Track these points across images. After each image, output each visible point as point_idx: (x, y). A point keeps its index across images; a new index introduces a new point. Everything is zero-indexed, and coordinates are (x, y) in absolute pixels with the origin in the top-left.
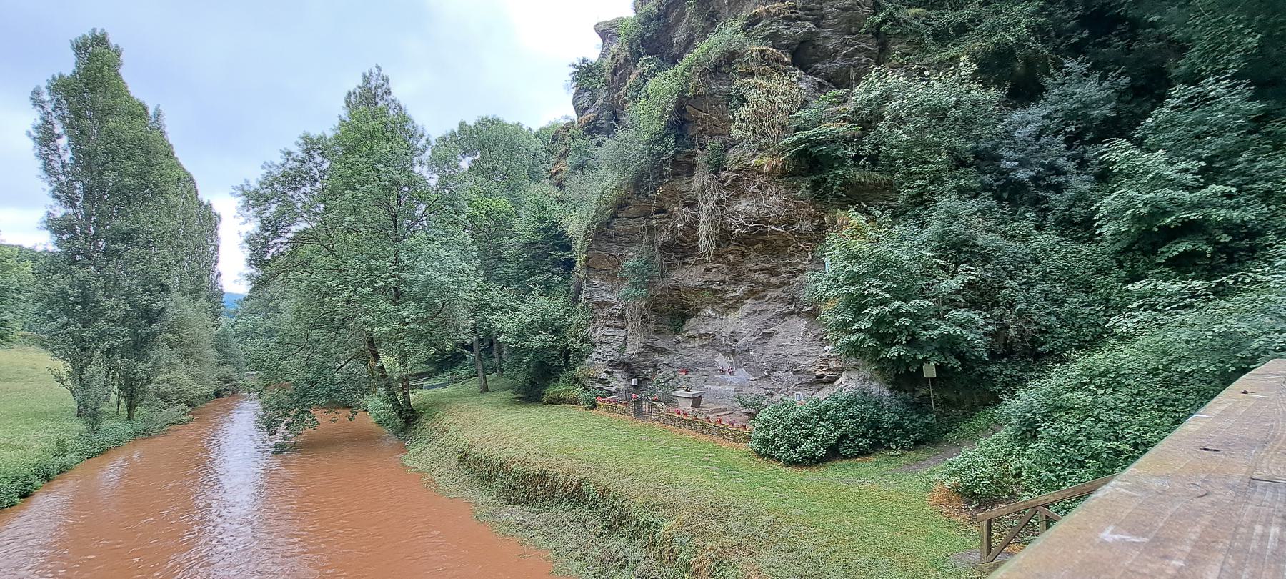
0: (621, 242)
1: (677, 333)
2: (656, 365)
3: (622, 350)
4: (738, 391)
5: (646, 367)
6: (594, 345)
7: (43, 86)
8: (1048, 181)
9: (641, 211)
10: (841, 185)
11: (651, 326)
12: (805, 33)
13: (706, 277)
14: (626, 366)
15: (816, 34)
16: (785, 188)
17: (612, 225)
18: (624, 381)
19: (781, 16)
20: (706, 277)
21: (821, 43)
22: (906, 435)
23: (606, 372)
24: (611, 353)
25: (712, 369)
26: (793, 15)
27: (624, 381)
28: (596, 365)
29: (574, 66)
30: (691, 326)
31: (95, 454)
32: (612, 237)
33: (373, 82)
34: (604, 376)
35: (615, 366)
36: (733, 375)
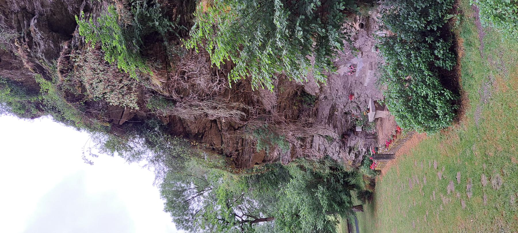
0: (242, 145)
1: (317, 99)
2: (346, 113)
3: (331, 140)
5: (347, 121)
6: (327, 157)
7: (188, 231)
9: (216, 135)
10: (170, 20)
11: (311, 120)
12: (40, 30)
14: (345, 137)
15: (41, 15)
16: (180, 61)
17: (229, 154)
18: (357, 138)
19: (29, 50)
21: (48, 9)
23: (349, 153)
25: (350, 78)
26: (27, 40)
27: (357, 138)
32: (239, 154)
34: (353, 156)
35: (344, 145)
36: (356, 65)
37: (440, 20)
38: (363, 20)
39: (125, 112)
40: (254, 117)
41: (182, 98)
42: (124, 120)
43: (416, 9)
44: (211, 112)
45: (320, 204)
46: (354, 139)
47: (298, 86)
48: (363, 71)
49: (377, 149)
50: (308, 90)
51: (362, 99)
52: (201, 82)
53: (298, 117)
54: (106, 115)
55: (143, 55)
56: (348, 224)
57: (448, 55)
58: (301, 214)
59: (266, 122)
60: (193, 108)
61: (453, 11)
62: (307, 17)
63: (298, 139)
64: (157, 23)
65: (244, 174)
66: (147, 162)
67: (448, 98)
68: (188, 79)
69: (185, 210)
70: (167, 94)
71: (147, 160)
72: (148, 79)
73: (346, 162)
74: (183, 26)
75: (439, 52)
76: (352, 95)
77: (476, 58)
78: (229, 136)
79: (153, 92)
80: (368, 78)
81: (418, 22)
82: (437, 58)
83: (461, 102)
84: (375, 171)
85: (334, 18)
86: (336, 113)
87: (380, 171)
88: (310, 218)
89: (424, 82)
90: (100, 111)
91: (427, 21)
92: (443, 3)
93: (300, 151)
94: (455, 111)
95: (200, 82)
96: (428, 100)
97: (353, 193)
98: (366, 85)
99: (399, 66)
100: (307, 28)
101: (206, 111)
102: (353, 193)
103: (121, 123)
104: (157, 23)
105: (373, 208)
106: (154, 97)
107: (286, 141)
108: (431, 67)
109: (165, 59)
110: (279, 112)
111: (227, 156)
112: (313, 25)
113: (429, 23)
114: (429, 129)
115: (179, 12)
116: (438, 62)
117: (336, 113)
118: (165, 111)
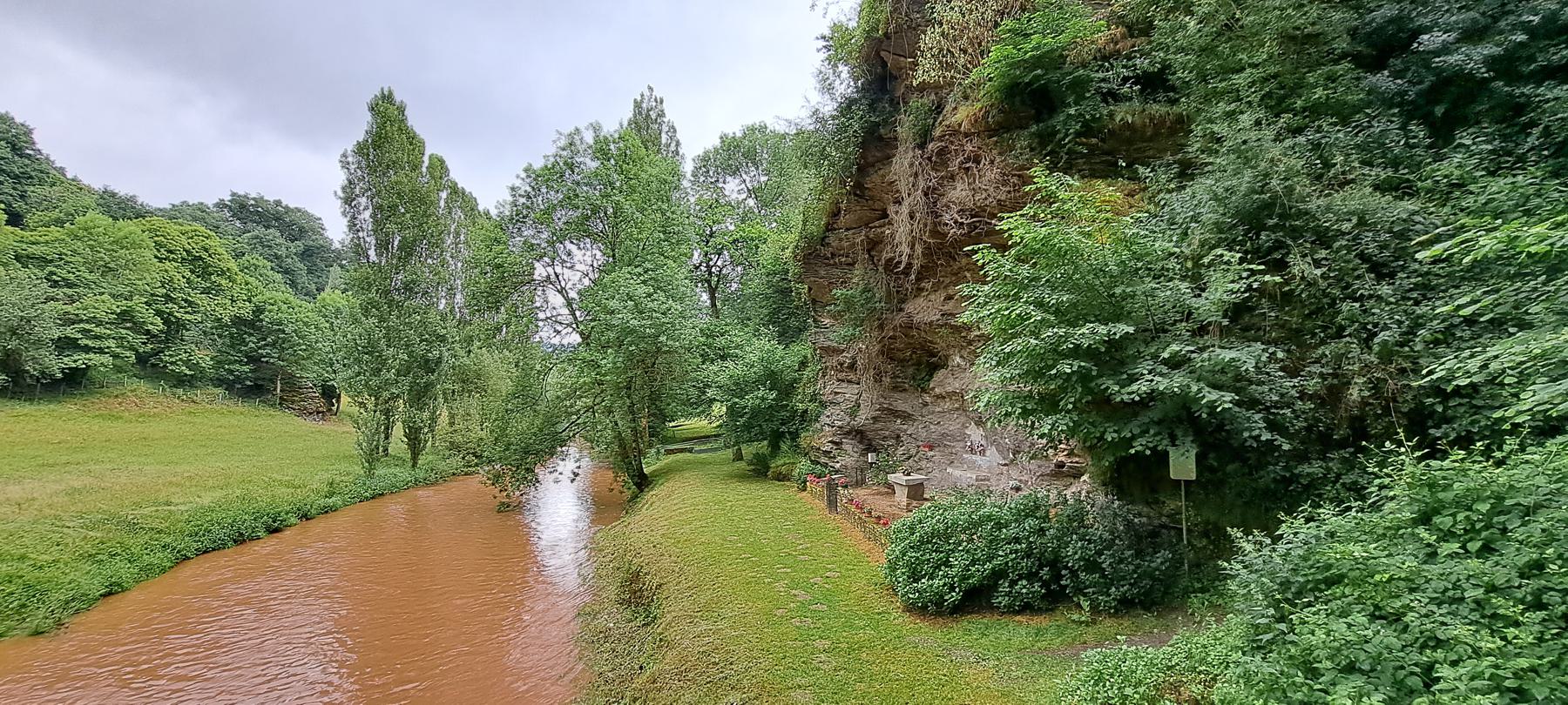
1: (924, 390)
2: (898, 436)
3: (853, 413)
4: (982, 480)
5: (885, 438)
6: (823, 405)
8: (1541, 60)
9: (860, 218)
10: (1078, 134)
13: (946, 308)
16: (1000, 154)
20: (946, 308)
22: (1108, 583)
24: (833, 417)
25: (962, 444)
28: (820, 436)
29: (824, 38)
30: (943, 381)
31: (367, 498)
33: (644, 105)
36: (984, 455)
37: (1079, 590)
38: (1070, 467)
39: (902, 59)
40: (892, 284)
41: (929, 159)
42: (890, 59)
43: (1099, 553)
44: (905, 209)
45: (747, 394)
46: (855, 449)
47: (947, 357)
48: (972, 466)
49: (845, 487)
50: (940, 375)
51: (923, 463)
52: (959, 192)
53: (891, 359)
54: (899, 25)
55: (1013, 87)
56: (709, 437)
57: (1018, 599)
58: (729, 364)
59: (883, 304)
60: (911, 179)
61: (1095, 609)
62: (1094, 378)
63: (853, 358)
64: (1072, 111)
65: (793, 269)
66: (813, 103)
67: (946, 598)
68: (964, 169)
69: (723, 169)
70: (937, 132)
71: (818, 103)
72: (966, 98)
73: (816, 437)
74: (1065, 157)
75: (1025, 587)
76: (931, 448)
77: (1016, 641)
78: (858, 240)
79: (939, 108)
80: (962, 475)
81: (1077, 557)
82: (1013, 583)
83: (940, 616)
84: (805, 482)
85: (1089, 423)
86: (899, 421)
87: (805, 489)
88: (723, 379)
89: (973, 563)
90: (906, 16)
91: (1077, 570)
92: (1110, 595)
93: (833, 361)
94: (925, 607)
95: (959, 189)
96: (943, 568)
97: (763, 446)
98: (949, 470)
99: (999, 526)
100: (1074, 379)
101: (906, 203)
102: (763, 446)
103: (883, 54)
104: (1072, 111)
105: (742, 477)
106: (930, 110)
107: (853, 338)
108: (998, 574)
109: (1003, 128)
110: (901, 325)
111: (823, 239)
112: (1080, 390)
113: (1074, 573)
114: (893, 568)
115: (1092, 148)
116: (1007, 584)
117: (899, 421)
118: (905, 128)
